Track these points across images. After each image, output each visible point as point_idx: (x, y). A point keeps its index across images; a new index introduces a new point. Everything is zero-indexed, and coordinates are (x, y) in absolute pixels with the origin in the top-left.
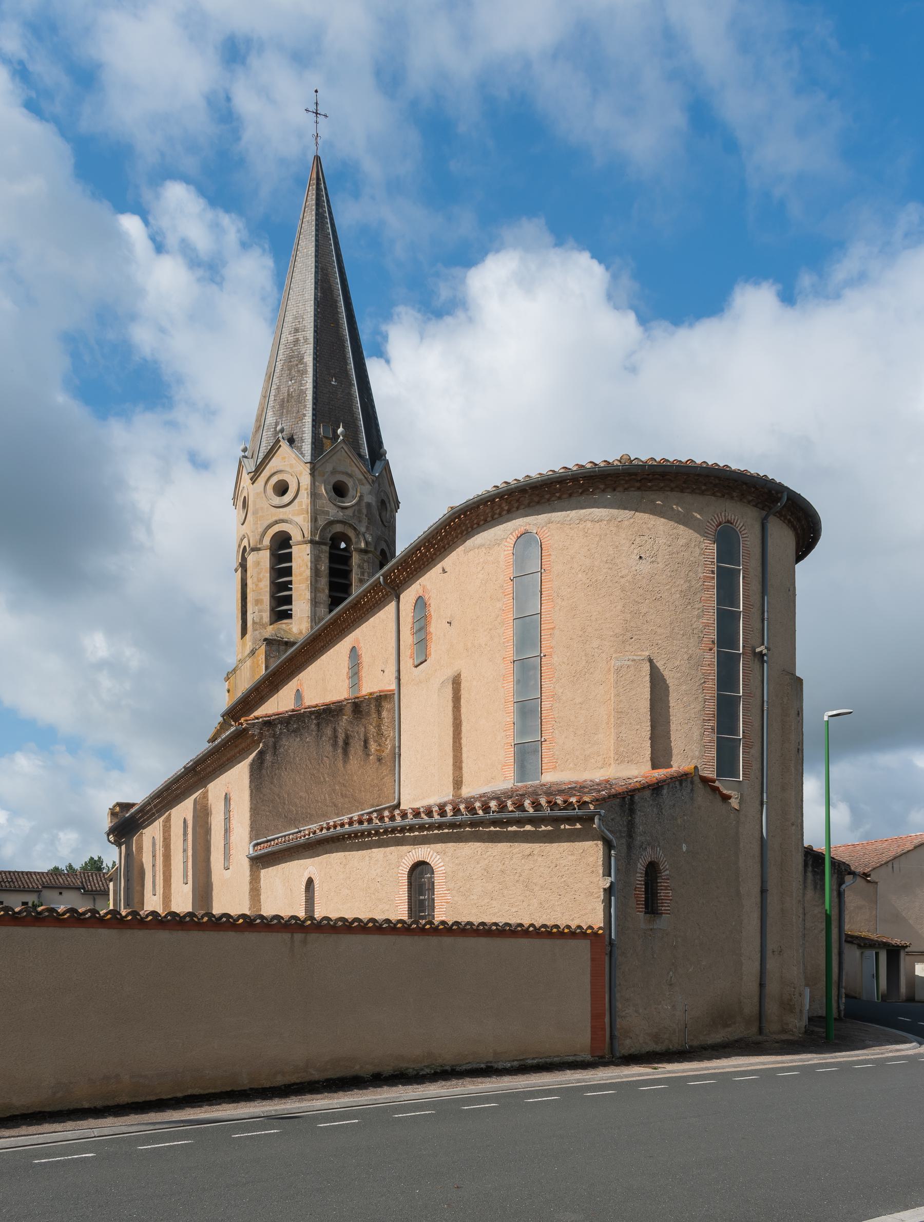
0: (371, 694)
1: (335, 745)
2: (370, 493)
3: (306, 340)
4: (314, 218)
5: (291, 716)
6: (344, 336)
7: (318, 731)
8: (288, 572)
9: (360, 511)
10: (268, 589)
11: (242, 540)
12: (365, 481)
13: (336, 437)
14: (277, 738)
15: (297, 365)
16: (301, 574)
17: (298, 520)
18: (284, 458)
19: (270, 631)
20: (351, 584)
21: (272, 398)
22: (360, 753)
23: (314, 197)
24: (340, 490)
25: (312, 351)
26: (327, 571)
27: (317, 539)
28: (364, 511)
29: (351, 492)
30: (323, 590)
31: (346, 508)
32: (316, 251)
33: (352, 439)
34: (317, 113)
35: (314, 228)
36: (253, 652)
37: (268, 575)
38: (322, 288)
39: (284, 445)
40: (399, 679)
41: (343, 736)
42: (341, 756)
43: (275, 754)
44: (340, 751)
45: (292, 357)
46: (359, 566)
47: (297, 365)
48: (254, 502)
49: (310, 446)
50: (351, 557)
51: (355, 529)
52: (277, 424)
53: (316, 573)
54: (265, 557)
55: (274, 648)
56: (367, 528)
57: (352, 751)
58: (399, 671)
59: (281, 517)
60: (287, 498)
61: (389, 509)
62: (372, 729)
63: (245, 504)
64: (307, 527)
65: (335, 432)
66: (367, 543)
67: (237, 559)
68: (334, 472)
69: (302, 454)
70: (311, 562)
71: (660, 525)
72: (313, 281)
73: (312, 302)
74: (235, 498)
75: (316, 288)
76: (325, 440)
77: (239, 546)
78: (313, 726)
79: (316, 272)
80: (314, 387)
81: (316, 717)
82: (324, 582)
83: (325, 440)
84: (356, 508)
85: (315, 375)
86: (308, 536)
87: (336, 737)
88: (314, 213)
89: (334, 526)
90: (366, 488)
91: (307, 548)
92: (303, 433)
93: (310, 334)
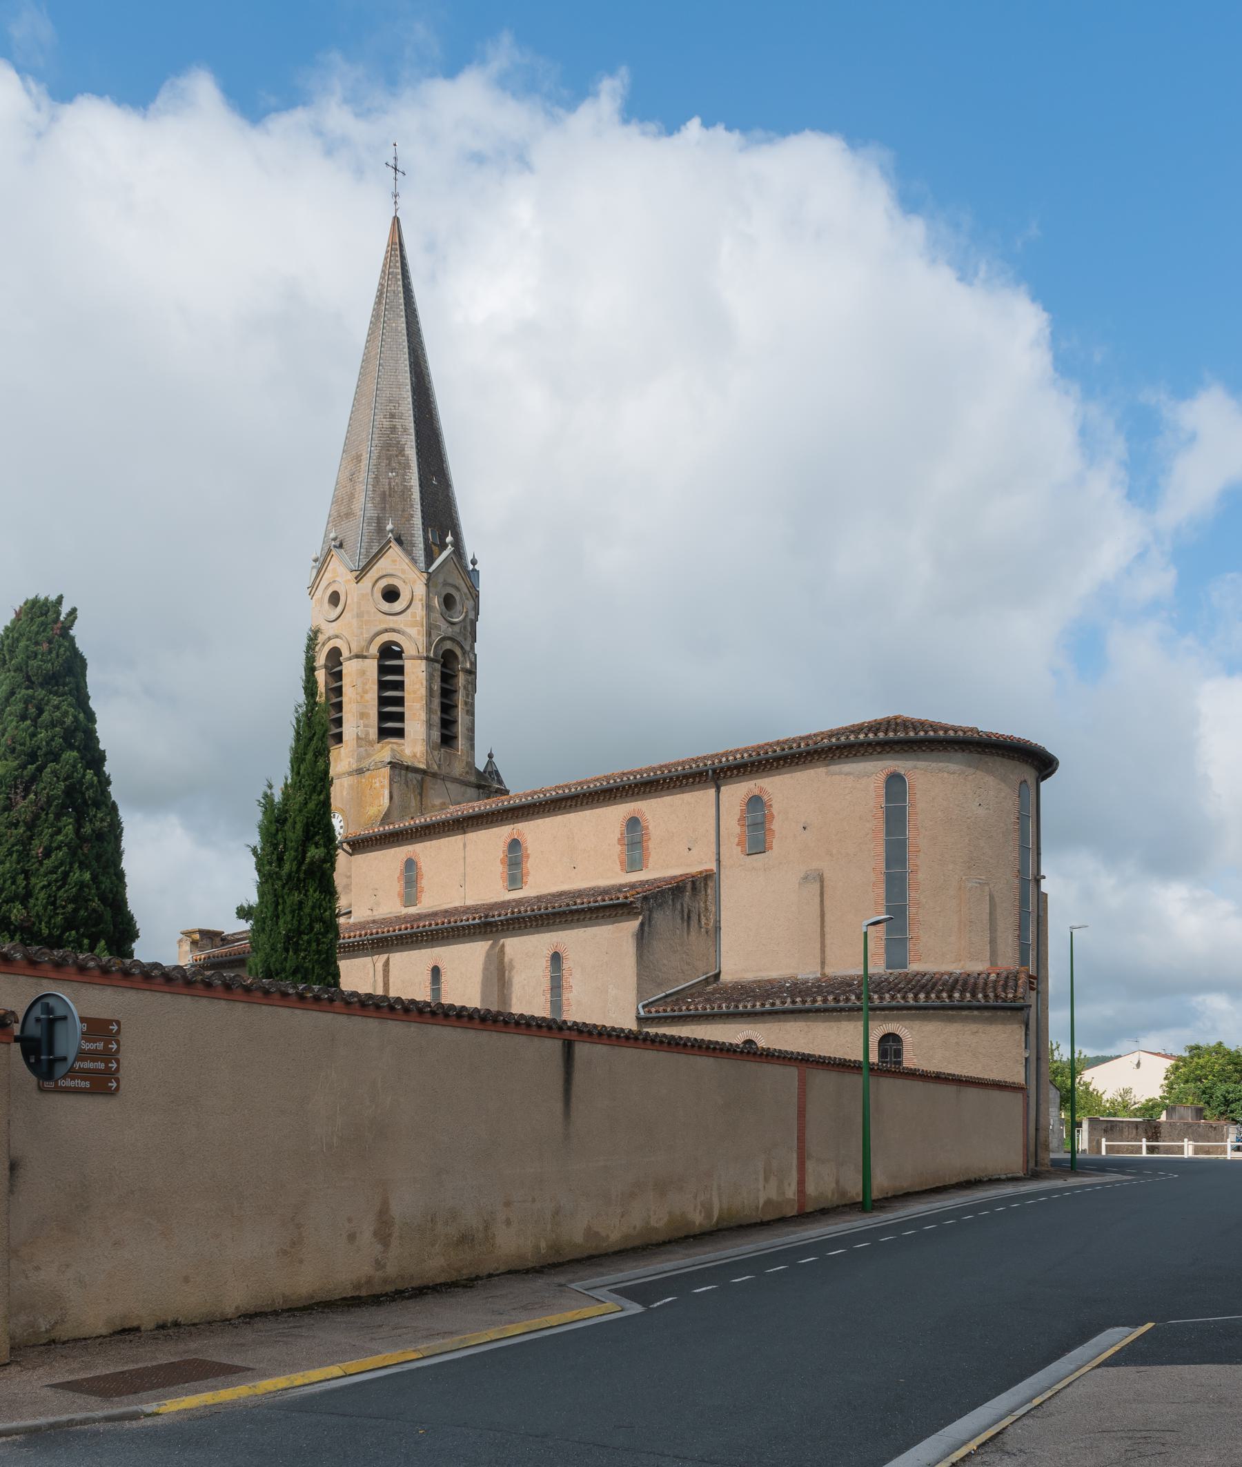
1: (682, 918)
3: (405, 430)
9: (465, 628)
14: (651, 911)
16: (415, 692)
20: (456, 706)
25: (414, 444)
29: (459, 607)
31: (453, 624)
39: (393, 544)
40: (719, 861)
46: (465, 688)
51: (462, 648)
54: (372, 666)
55: (397, 772)
58: (719, 854)
59: (392, 625)
60: (398, 606)
62: (702, 905)
64: (422, 641)
68: (446, 584)
71: (990, 780)
74: (313, 588)
82: (437, 702)
91: (423, 665)
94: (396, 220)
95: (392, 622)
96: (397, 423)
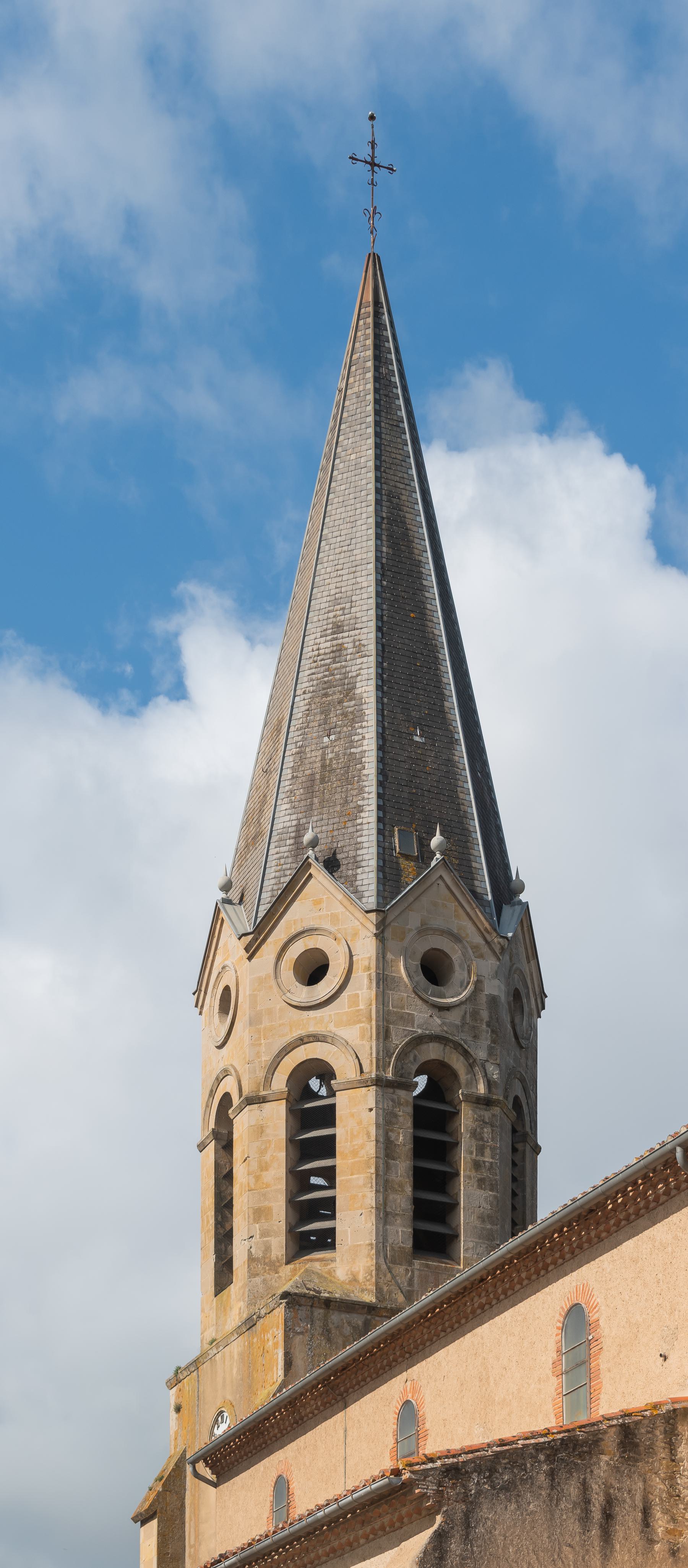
0: (656, 1406)
1: (585, 1518)
2: (496, 975)
3: (359, 648)
4: (370, 386)
5: (497, 1455)
6: (435, 637)
7: (552, 1487)
8: (327, 1147)
9: (475, 1015)
10: (282, 1186)
11: (219, 1080)
12: (485, 950)
13: (426, 855)
14: (471, 1504)
15: (340, 702)
16: (355, 1153)
17: (349, 1034)
18: (317, 902)
19: (289, 1277)
20: (457, 1174)
21: (288, 773)
22: (635, 1536)
23: (370, 342)
24: (433, 970)
25: (373, 671)
26: (410, 1146)
27: (390, 1075)
28: (485, 1014)
29: (459, 974)
30: (401, 1185)
31: (447, 1008)
32: (378, 457)
33: (459, 860)
34: (373, 164)
35: (370, 408)
36: (250, 1324)
37: (282, 1155)
38: (390, 536)
39: (318, 873)
41: (602, 1498)
42: (597, 1543)
43: (466, 1538)
44: (595, 1532)
45: (330, 685)
46: (474, 1134)
47: (340, 702)
48: (253, 999)
49: (373, 876)
50: (456, 1114)
51: (466, 1054)
52: (300, 830)
53: (387, 1149)
54: (275, 1117)
55: (303, 1312)
56: (491, 1052)
57: (619, 1532)
59: (312, 1029)
60: (324, 989)
61: (526, 1009)
62: (659, 1485)
63: (226, 1001)
64: (368, 1049)
65: (424, 844)
66: (490, 1084)
67: (206, 1121)
68: (424, 930)
69: (356, 892)
70: (378, 1126)
72: (372, 521)
73: (371, 567)
74: (200, 990)
75: (378, 537)
76: (403, 863)
77: (212, 1094)
78: (542, 1477)
79: (378, 502)
80: (380, 748)
81: (548, 1457)
82: (403, 1168)
83: (403, 863)
84: (468, 1007)
85: (380, 723)
86: (371, 1071)
87: (587, 1502)
88: (370, 375)
89: (424, 1047)
90: (487, 965)
91: (369, 1096)
92: (358, 846)
93: (368, 635)
94: (375, 260)
95: (313, 1022)
96: (347, 639)
